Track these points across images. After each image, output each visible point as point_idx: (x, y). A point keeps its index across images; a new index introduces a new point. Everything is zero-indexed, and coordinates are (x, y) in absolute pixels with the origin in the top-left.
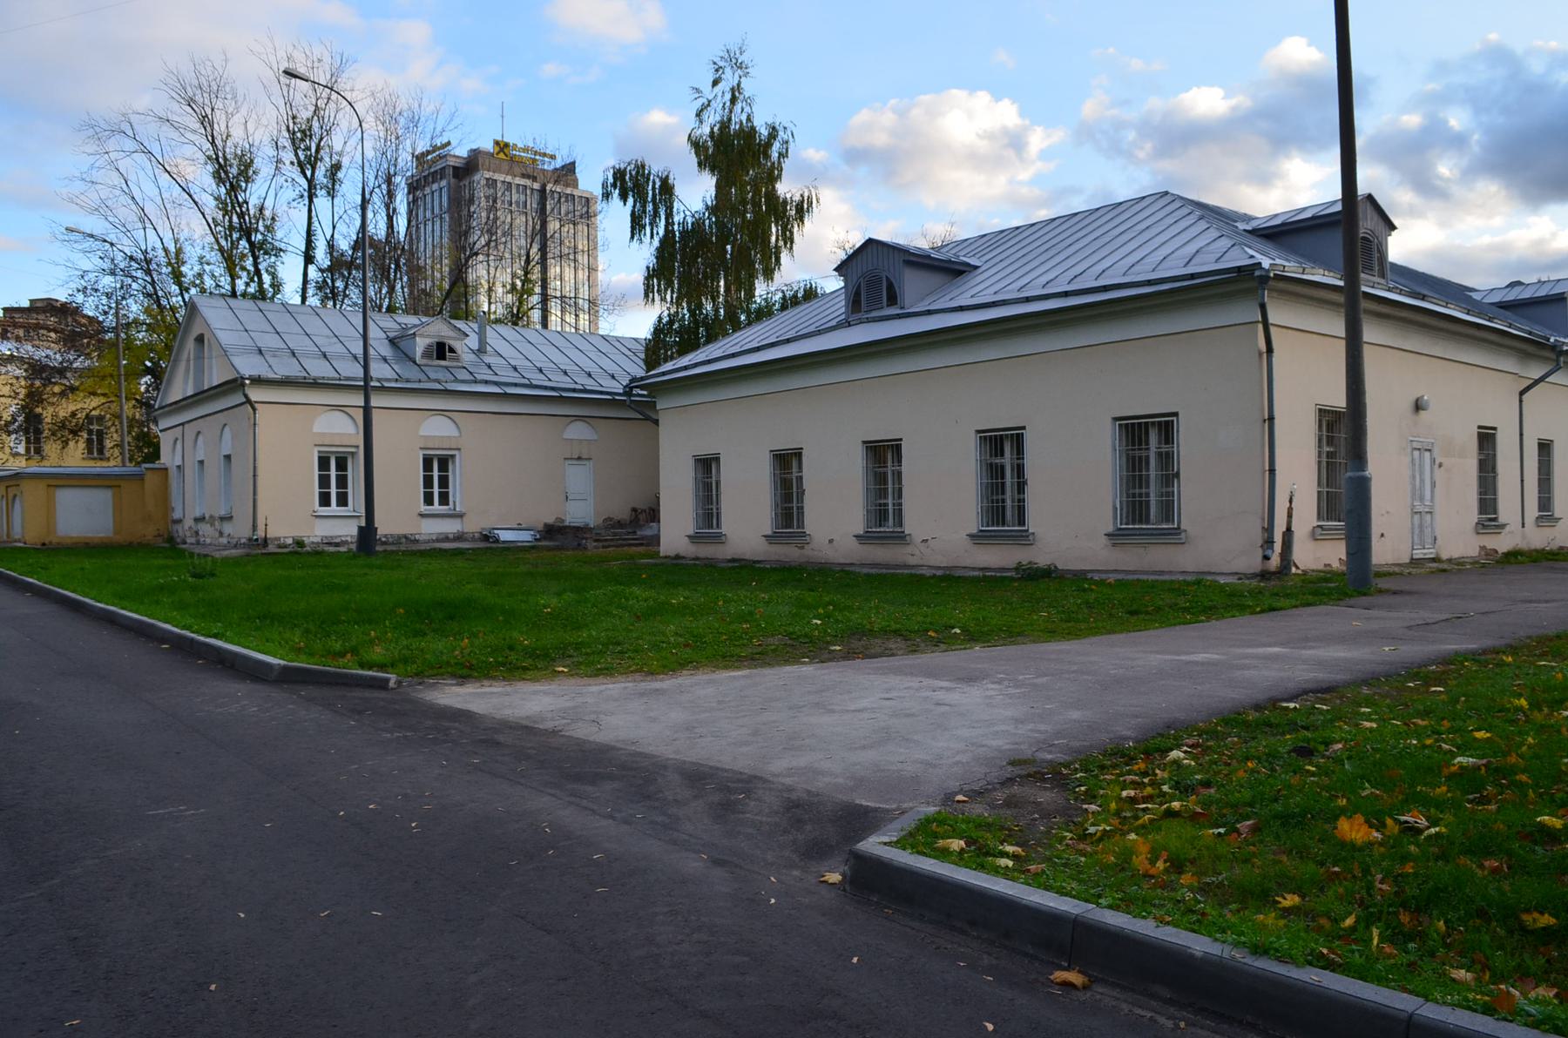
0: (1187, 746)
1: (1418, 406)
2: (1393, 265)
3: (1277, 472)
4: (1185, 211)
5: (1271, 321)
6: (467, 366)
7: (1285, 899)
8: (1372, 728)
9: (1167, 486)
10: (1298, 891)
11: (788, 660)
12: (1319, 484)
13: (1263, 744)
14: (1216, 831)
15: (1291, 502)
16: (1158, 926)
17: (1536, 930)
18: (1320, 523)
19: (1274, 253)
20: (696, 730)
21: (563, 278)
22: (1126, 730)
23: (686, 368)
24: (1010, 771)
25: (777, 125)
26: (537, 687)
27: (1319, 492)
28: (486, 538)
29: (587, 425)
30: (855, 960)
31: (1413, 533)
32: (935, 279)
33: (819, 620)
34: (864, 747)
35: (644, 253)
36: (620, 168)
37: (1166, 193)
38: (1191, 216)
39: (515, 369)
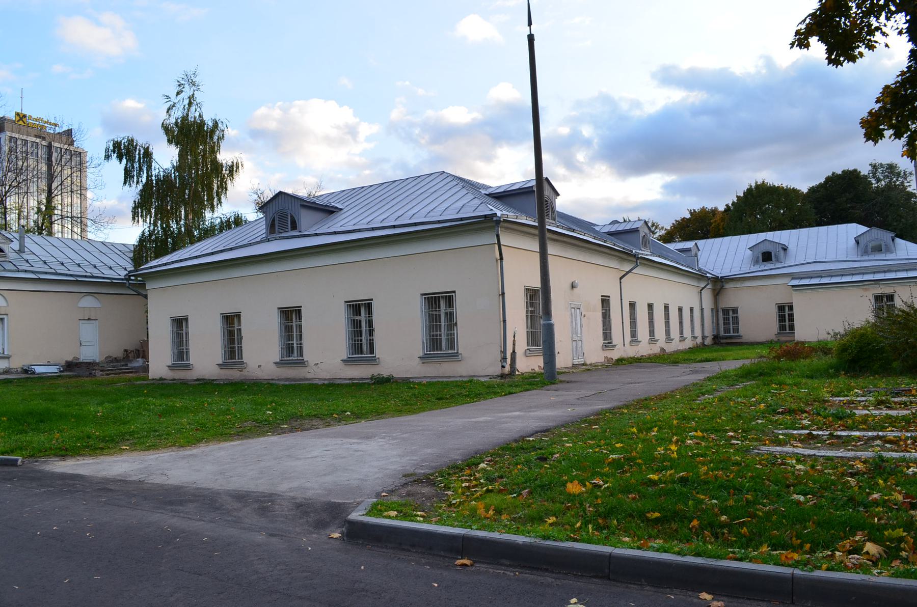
0: (487, 461)
1: (573, 286)
2: (558, 212)
3: (507, 322)
4: (454, 183)
5: (502, 243)
6: (11, 261)
7: (550, 519)
8: (570, 446)
9: (451, 330)
10: (554, 515)
11: (259, 435)
12: (527, 328)
13: (522, 457)
14: (513, 496)
15: (514, 337)
16: (500, 534)
17: (653, 519)
18: (528, 348)
19: (501, 207)
20: (226, 474)
21: (63, 202)
22: (456, 456)
23: (166, 264)
24: (404, 480)
25: (217, 120)
26: (114, 458)
27: (527, 331)
28: (26, 371)
29: (94, 298)
30: (362, 568)
31: (573, 351)
32: (319, 215)
33: (270, 411)
34: (325, 475)
35: (133, 192)
36: (117, 141)
37: (444, 172)
38: (458, 186)
39: (45, 263)
